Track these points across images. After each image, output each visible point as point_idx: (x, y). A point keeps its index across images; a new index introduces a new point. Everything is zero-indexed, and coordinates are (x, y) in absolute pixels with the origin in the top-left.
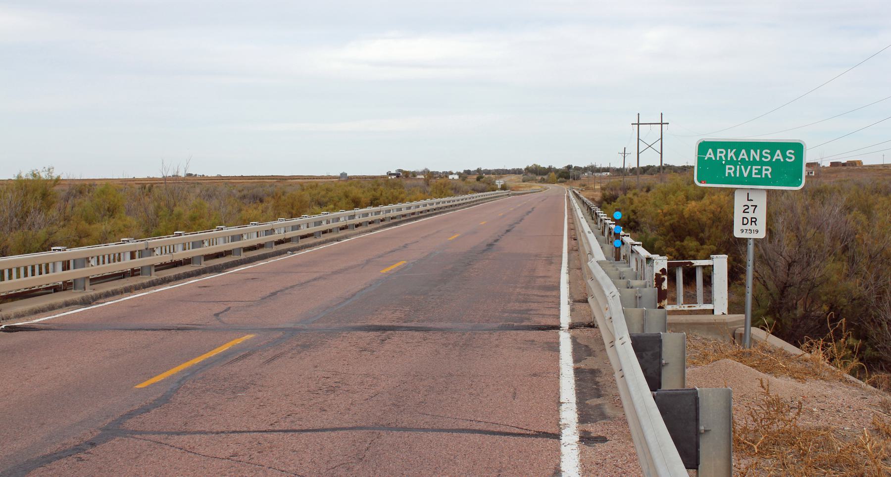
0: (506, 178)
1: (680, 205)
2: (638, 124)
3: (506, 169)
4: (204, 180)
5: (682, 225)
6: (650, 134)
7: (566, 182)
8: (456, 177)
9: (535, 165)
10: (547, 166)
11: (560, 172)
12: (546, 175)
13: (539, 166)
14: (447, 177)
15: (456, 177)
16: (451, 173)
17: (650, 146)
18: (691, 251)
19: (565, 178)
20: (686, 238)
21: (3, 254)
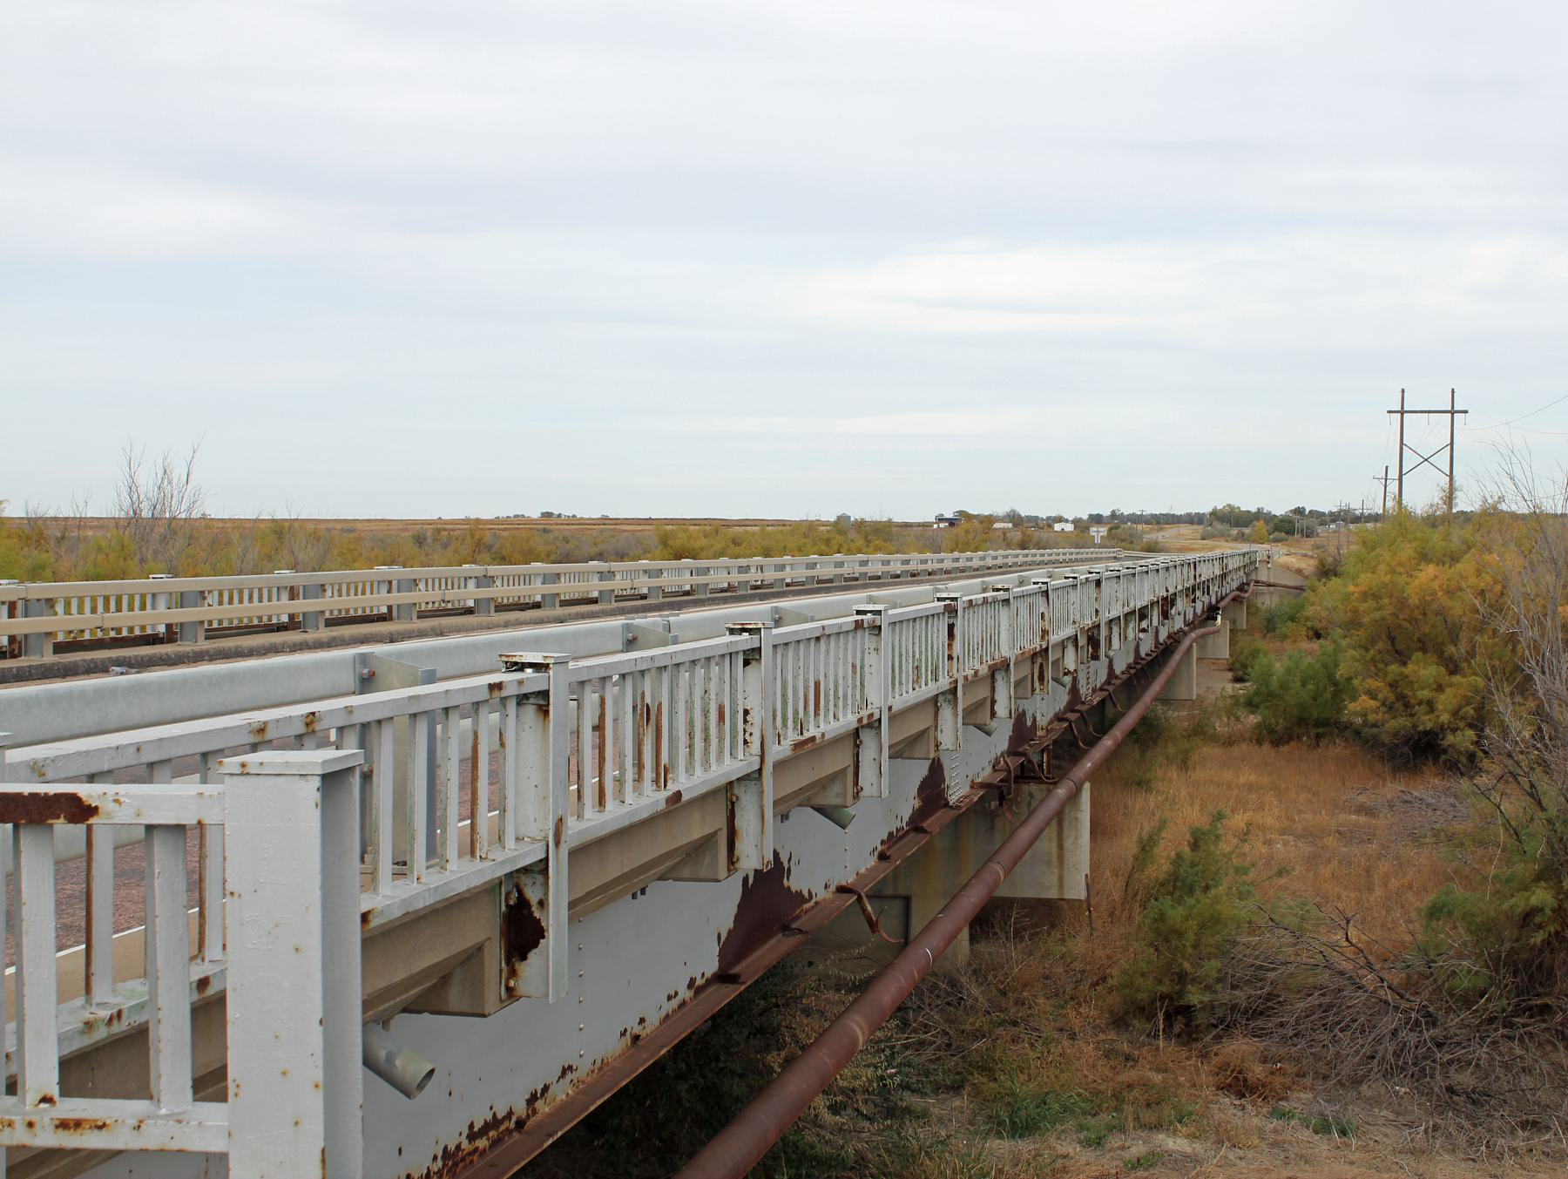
0: (1169, 531)
1: (1401, 574)
2: (1402, 412)
3: (1172, 513)
4: (568, 524)
5: (1406, 624)
6: (1426, 434)
7: (1287, 540)
8: (1069, 527)
9: (1229, 505)
10: (1253, 509)
11: (1276, 521)
12: (1247, 527)
13: (1239, 508)
14: (1050, 526)
15: (1069, 527)
16: (1060, 519)
17: (1427, 460)
18: (1423, 688)
19: (1287, 533)
20: (1414, 657)
21: (4, 657)
